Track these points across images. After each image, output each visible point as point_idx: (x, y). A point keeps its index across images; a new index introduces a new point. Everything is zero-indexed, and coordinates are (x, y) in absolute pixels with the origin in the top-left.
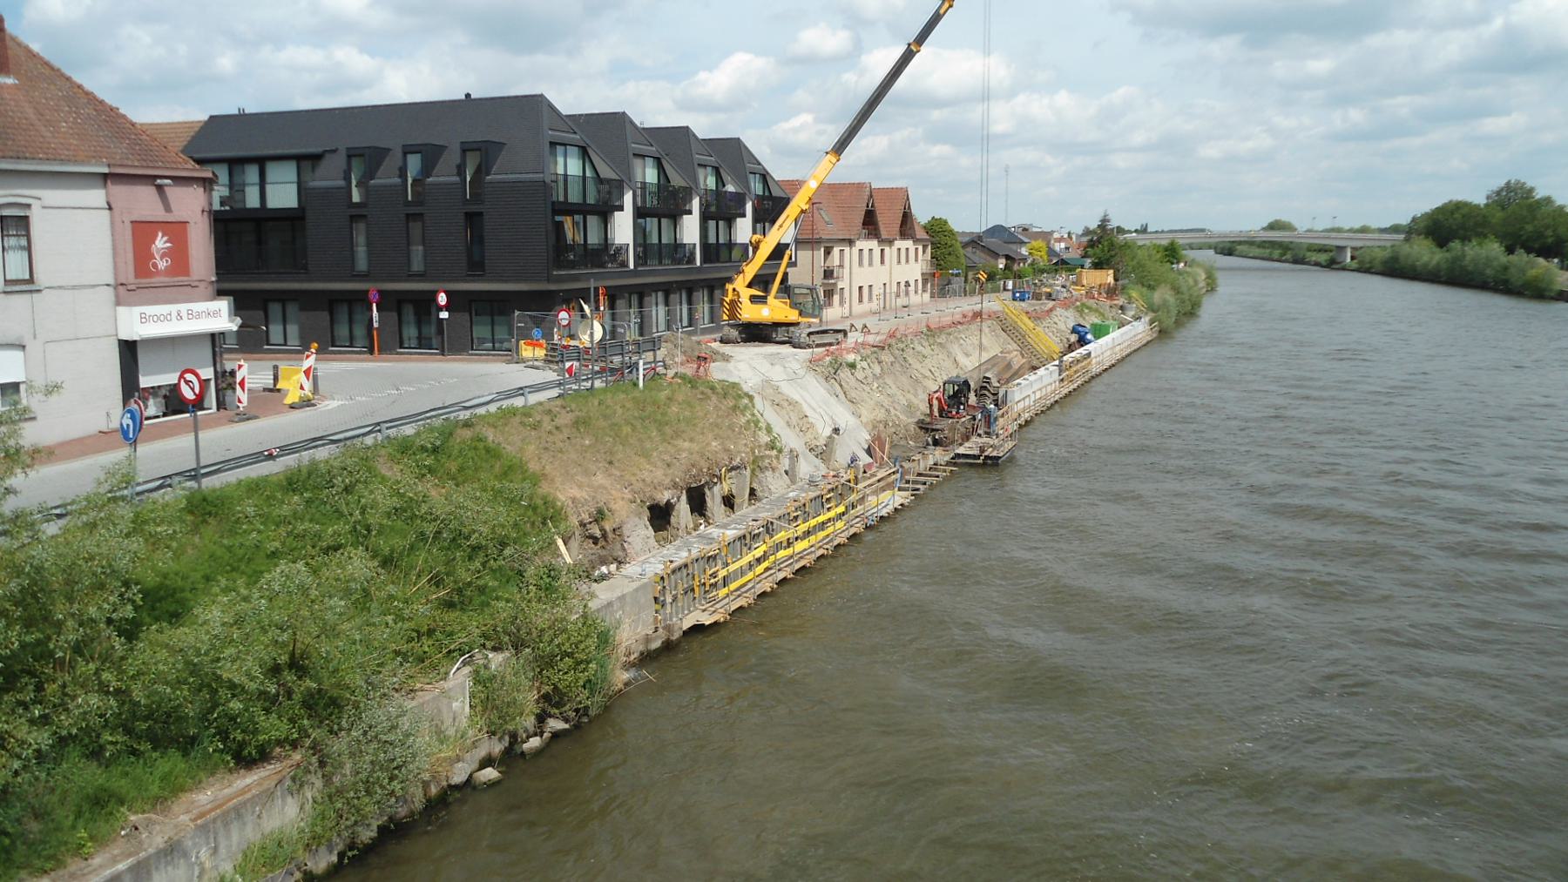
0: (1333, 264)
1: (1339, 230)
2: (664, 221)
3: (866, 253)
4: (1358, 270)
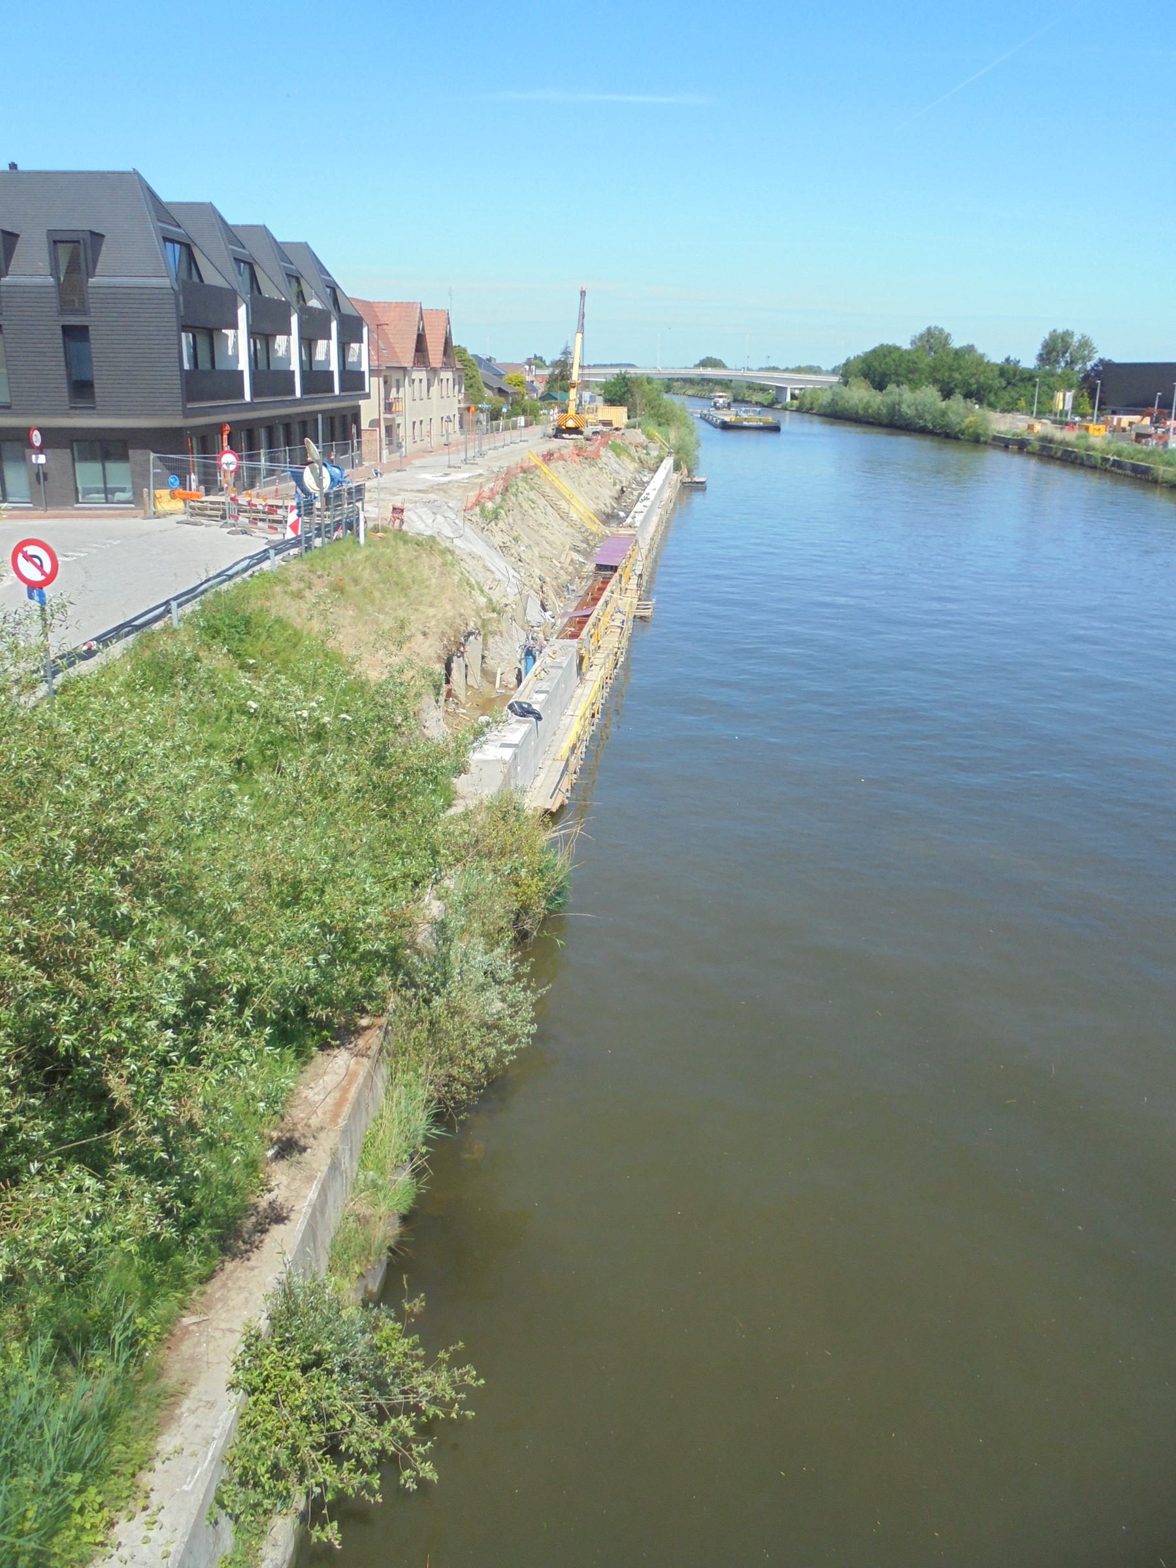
1: (775, 369)
4: (799, 410)
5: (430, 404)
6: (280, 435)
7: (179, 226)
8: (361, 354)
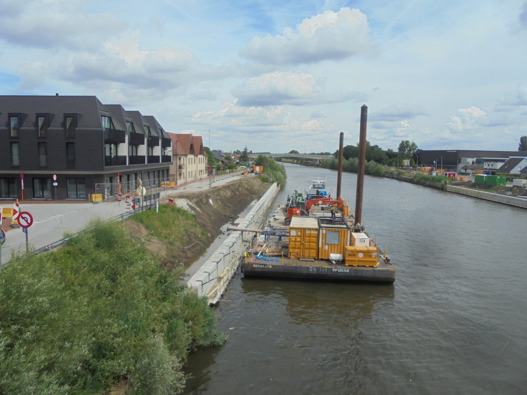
1: (314, 154)
5: (194, 166)
6: (161, 173)
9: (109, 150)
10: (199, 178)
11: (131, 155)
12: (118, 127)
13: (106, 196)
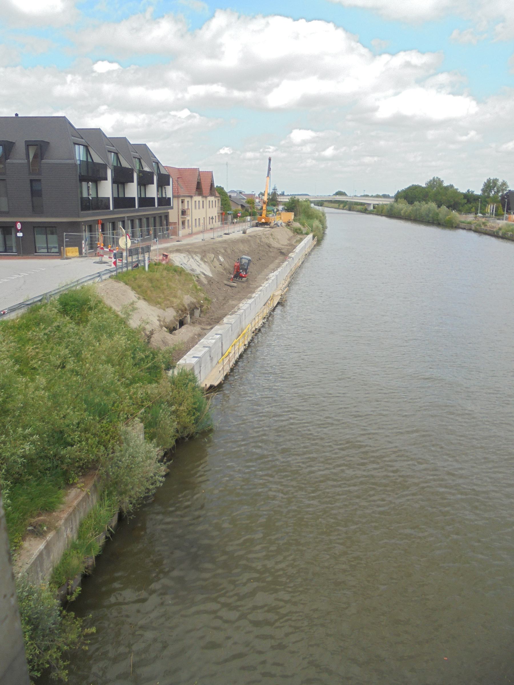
0: (365, 211)
1: (367, 196)
2: (120, 185)
3: (197, 202)
4: (377, 214)
5: (203, 211)
7: (83, 138)
8: (169, 192)
9: (87, 191)
10: (209, 227)
11: (139, 196)
12: (97, 159)
13: (84, 250)
